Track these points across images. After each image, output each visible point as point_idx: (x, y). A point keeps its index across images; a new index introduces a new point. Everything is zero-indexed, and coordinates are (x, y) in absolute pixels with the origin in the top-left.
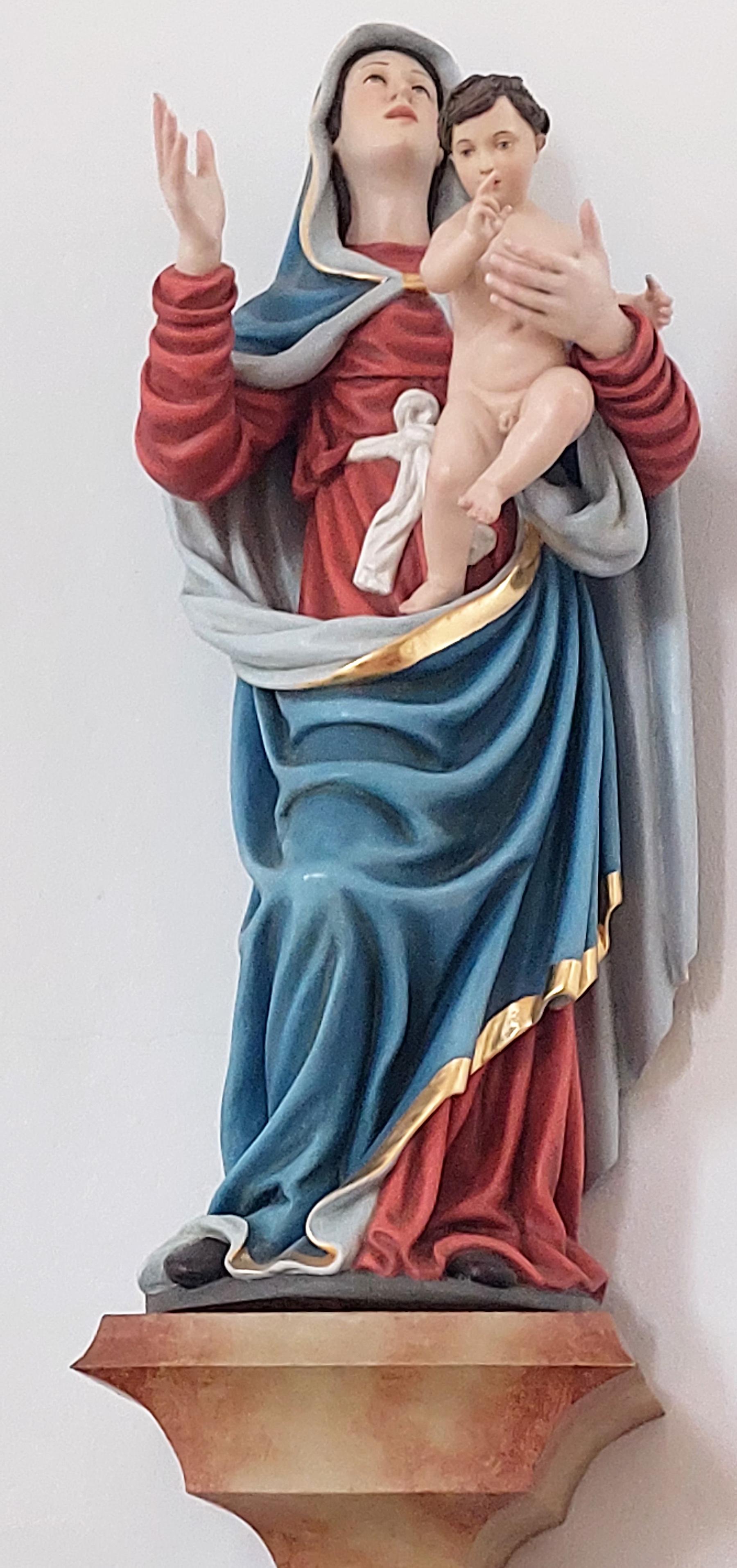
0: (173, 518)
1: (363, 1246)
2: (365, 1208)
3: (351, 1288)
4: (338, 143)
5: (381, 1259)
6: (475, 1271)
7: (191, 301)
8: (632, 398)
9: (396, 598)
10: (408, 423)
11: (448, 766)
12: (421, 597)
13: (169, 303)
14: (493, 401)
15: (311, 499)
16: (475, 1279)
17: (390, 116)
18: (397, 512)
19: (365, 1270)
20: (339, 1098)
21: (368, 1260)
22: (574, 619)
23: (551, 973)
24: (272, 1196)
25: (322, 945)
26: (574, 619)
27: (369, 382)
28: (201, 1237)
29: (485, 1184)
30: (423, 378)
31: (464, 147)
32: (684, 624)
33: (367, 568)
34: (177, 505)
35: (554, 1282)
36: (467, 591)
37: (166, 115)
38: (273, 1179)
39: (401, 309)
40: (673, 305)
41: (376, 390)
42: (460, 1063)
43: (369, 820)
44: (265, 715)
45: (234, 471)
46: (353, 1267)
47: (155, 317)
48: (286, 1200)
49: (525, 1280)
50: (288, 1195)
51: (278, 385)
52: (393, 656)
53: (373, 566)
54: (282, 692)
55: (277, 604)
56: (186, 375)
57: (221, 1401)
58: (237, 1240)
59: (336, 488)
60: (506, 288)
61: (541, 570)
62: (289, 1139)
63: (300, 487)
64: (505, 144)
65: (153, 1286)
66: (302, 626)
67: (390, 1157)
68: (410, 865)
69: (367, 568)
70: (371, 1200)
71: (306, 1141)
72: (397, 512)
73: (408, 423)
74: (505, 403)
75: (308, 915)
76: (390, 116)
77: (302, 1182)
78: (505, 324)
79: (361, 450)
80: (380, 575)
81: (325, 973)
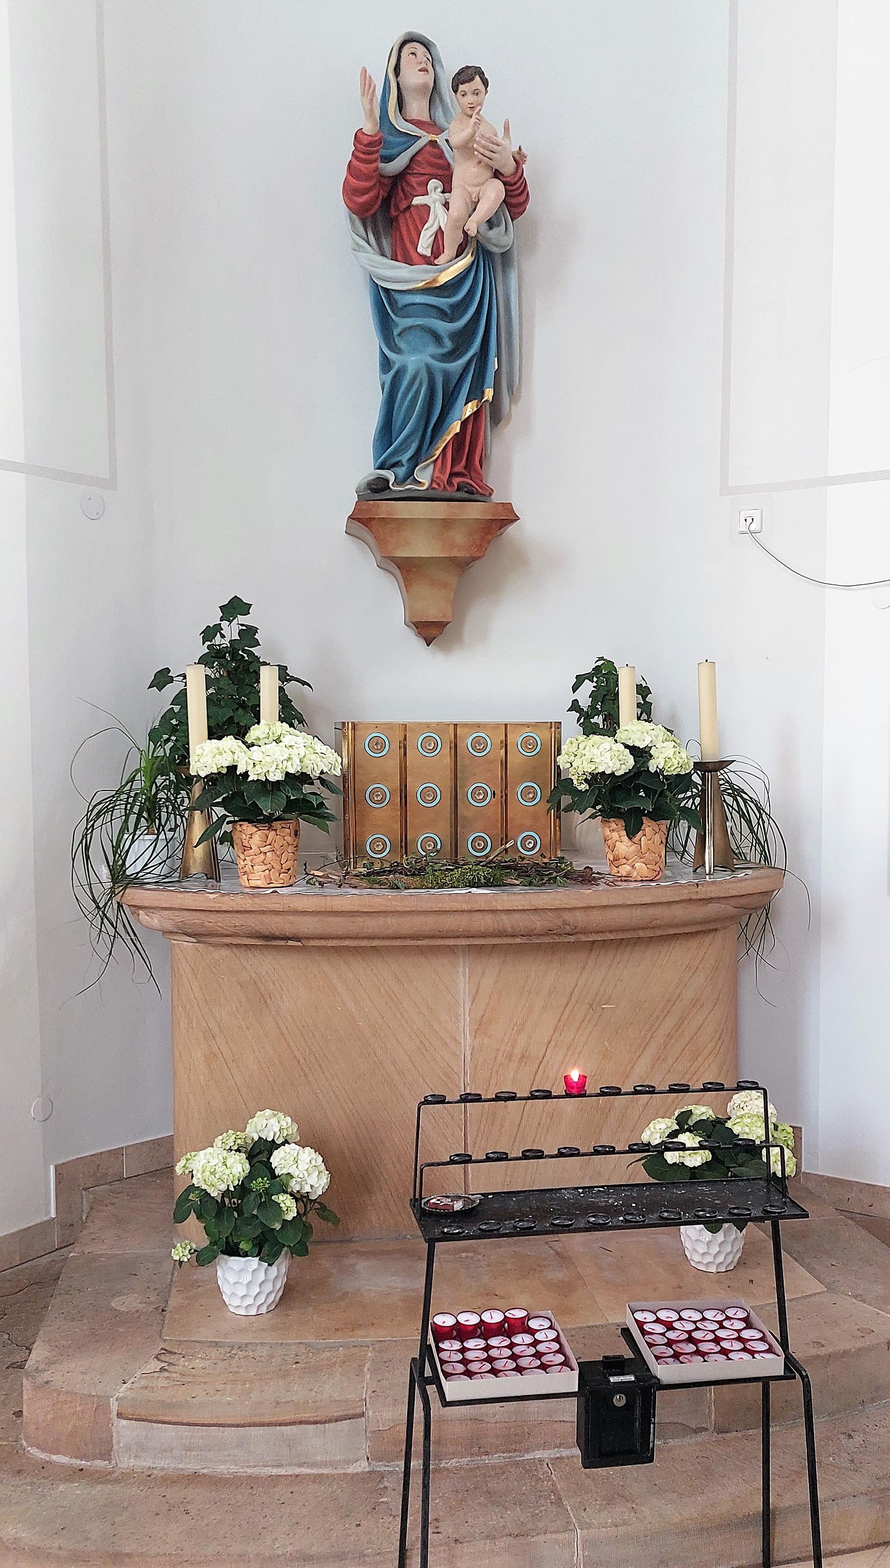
0: (348, 221)
1: (432, 481)
2: (431, 469)
3: (431, 493)
4: (399, 79)
5: (439, 485)
6: (466, 489)
7: (369, 145)
8: (514, 190)
9: (432, 258)
10: (433, 192)
11: (451, 321)
12: (442, 259)
13: (361, 144)
14: (470, 189)
15: (397, 217)
16: (466, 492)
17: (420, 70)
18: (431, 226)
19: (434, 488)
20: (421, 430)
21: (434, 485)
22: (487, 268)
23: (483, 393)
24: (397, 464)
25: (418, 380)
26: (487, 268)
27: (418, 175)
28: (377, 477)
29: (461, 461)
30: (437, 175)
31: (463, 93)
32: (516, 270)
33: (423, 247)
34: (350, 215)
35: (484, 493)
36: (457, 256)
37: (367, 75)
38: (399, 459)
39: (429, 148)
40: (528, 158)
41: (423, 178)
42: (458, 423)
43: (428, 338)
44: (385, 297)
45: (376, 207)
46: (430, 487)
47: (354, 148)
48: (403, 465)
49: (478, 492)
50: (404, 464)
51: (391, 175)
52: (435, 280)
53: (425, 246)
54: (393, 290)
55: (383, 254)
56: (366, 172)
57: (393, 529)
58: (392, 479)
59: (407, 215)
60: (481, 150)
61: (477, 250)
62: (404, 446)
63: (393, 213)
64: (477, 94)
65: (360, 492)
66: (400, 267)
67: (438, 452)
68: (444, 355)
69: (423, 247)
70: (432, 466)
71: (409, 446)
72: (431, 226)
73: (433, 192)
74: (474, 190)
75: (414, 371)
76: (420, 70)
77: (409, 460)
78: (475, 162)
79: (417, 201)
80: (427, 249)
81: (418, 392)
